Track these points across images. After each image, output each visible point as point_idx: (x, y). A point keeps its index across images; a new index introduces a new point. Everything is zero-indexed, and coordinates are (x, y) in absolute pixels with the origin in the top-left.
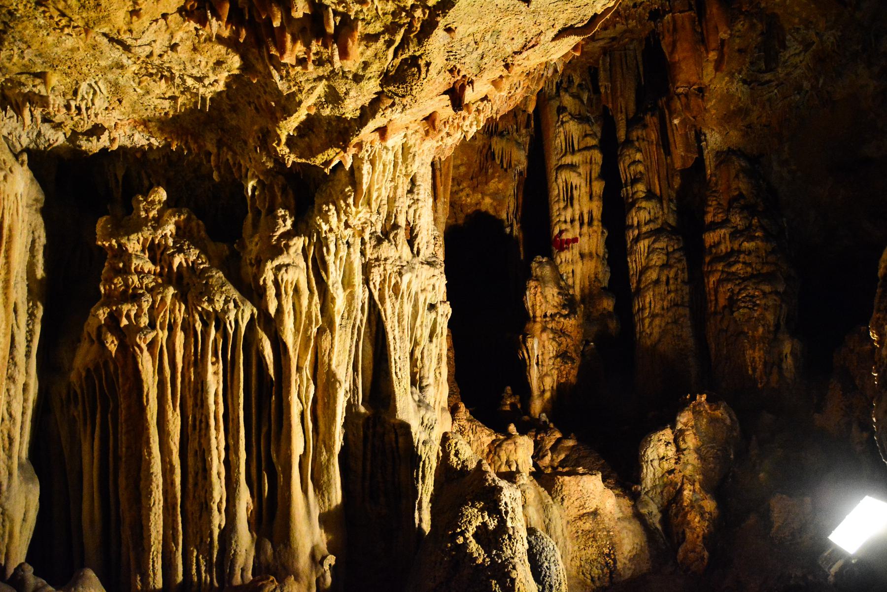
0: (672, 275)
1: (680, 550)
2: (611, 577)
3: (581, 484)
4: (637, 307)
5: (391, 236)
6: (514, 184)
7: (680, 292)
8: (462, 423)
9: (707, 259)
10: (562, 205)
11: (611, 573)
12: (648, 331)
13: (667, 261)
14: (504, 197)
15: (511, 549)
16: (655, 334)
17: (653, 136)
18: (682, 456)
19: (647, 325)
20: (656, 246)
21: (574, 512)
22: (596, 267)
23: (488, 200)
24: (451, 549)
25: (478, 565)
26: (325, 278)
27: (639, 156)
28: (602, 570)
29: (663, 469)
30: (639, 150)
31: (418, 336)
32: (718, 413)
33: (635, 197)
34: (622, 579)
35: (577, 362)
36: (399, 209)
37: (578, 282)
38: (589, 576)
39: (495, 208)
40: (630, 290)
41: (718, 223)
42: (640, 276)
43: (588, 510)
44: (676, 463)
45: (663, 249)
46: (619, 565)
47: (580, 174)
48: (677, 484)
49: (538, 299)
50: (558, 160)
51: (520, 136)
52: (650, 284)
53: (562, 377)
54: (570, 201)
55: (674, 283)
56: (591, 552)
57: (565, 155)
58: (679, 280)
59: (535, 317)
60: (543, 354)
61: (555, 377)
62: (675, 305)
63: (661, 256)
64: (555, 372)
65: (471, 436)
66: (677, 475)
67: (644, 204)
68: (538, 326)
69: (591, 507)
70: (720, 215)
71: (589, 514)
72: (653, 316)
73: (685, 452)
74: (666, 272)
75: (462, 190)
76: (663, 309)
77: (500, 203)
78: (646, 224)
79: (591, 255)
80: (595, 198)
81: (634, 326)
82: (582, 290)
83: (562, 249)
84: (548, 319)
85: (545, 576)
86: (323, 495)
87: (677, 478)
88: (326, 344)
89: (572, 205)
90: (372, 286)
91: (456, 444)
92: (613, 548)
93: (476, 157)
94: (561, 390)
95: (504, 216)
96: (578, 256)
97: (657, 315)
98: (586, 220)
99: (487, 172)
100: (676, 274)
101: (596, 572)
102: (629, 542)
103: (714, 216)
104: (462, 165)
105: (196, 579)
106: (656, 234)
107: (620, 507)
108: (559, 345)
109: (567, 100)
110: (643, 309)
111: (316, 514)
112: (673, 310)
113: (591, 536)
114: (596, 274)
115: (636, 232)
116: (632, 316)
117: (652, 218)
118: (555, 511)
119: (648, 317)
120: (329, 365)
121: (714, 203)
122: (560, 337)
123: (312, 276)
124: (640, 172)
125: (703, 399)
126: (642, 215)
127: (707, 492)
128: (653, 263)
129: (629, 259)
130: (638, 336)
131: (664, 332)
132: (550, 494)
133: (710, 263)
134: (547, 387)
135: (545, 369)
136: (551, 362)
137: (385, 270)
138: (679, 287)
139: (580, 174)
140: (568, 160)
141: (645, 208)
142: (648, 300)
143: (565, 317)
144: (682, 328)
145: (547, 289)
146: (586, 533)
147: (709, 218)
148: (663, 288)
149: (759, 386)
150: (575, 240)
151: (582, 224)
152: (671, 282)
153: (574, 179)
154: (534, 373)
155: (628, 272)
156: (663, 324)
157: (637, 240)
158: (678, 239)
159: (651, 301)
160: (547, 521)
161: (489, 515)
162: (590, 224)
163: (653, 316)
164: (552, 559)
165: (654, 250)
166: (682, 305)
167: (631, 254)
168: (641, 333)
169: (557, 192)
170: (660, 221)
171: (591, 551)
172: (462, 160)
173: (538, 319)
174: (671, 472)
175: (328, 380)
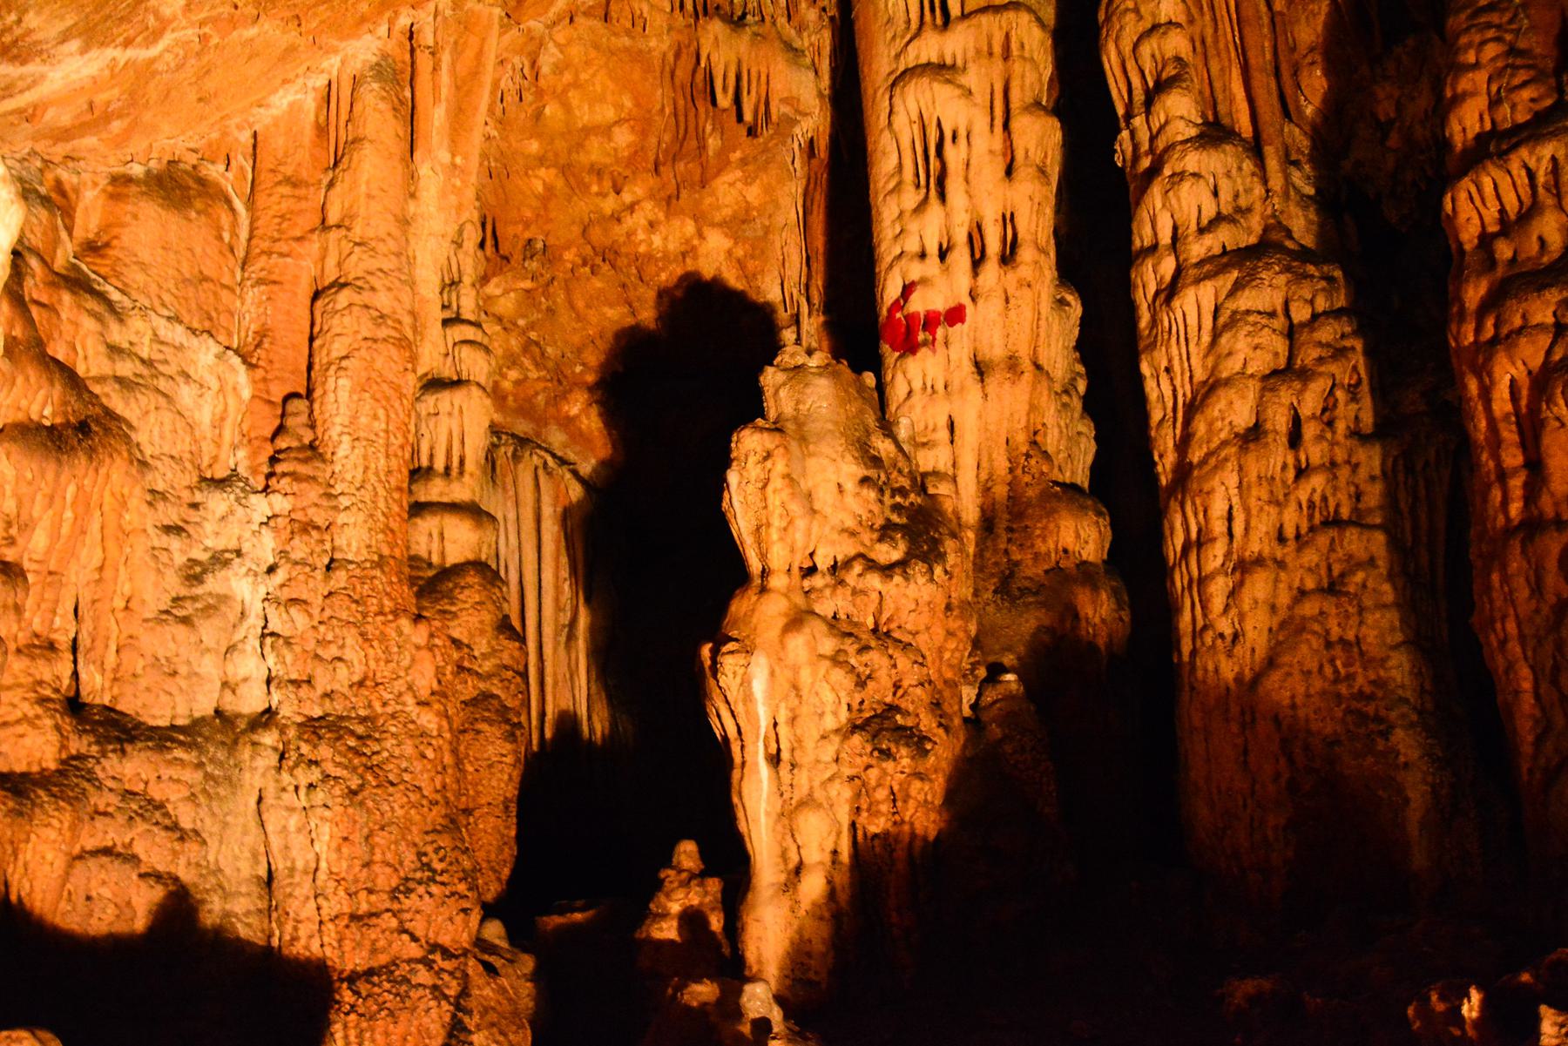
0: (1310, 403)
4: (1179, 540)
6: (796, 188)
7: (1344, 473)
9: (1474, 293)
10: (911, 198)
13: (1291, 357)
14: (767, 230)
16: (1251, 634)
19: (1218, 603)
20: (1245, 301)
22: (1033, 408)
33: (1161, 144)
34: (824, 986)
35: (944, 751)
37: (968, 461)
39: (741, 264)
40: (1156, 478)
41: (1517, 128)
42: (1187, 422)
49: (774, 501)
50: (898, 56)
51: (800, 29)
52: (1224, 443)
53: (873, 812)
55: (1320, 438)
58: (1341, 426)
59: (765, 573)
60: (793, 720)
62: (1326, 523)
63: (1265, 337)
64: (842, 794)
67: (1192, 161)
70: (1526, 94)
72: (1243, 567)
74: (1286, 396)
75: (631, 208)
76: (1281, 539)
77: (759, 247)
78: (1201, 231)
80: (1023, 172)
81: (1170, 610)
83: (909, 347)
84: (818, 581)
89: (942, 196)
93: (660, 96)
94: (873, 869)
95: (773, 294)
96: (968, 367)
97: (1259, 561)
98: (993, 246)
99: (702, 147)
100: (1329, 406)
103: (1494, 103)
108: (861, 683)
110: (1201, 542)
112: (1323, 540)
115: (1168, 266)
116: (1163, 572)
117: (1226, 209)
119: (1222, 569)
121: (1491, 50)
122: (865, 649)
124: (1178, 59)
126: (1189, 199)
128: (1234, 365)
129: (1145, 369)
130: (1186, 646)
131: (1289, 629)
133: (1493, 302)
135: (802, 778)
136: (828, 752)
138: (1340, 455)
140: (930, 48)
142: (1218, 508)
143: (887, 570)
144: (1361, 610)
145: (812, 463)
147: (1468, 122)
148: (1277, 456)
150: (955, 315)
152: (1310, 431)
153: (944, 105)
155: (1145, 416)
156: (1284, 599)
157: (1170, 291)
158: (1330, 279)
165: (1235, 319)
166: (1358, 521)
167: (1152, 346)
168: (1197, 634)
170: (1256, 222)
172: (619, 107)
173: (777, 582)
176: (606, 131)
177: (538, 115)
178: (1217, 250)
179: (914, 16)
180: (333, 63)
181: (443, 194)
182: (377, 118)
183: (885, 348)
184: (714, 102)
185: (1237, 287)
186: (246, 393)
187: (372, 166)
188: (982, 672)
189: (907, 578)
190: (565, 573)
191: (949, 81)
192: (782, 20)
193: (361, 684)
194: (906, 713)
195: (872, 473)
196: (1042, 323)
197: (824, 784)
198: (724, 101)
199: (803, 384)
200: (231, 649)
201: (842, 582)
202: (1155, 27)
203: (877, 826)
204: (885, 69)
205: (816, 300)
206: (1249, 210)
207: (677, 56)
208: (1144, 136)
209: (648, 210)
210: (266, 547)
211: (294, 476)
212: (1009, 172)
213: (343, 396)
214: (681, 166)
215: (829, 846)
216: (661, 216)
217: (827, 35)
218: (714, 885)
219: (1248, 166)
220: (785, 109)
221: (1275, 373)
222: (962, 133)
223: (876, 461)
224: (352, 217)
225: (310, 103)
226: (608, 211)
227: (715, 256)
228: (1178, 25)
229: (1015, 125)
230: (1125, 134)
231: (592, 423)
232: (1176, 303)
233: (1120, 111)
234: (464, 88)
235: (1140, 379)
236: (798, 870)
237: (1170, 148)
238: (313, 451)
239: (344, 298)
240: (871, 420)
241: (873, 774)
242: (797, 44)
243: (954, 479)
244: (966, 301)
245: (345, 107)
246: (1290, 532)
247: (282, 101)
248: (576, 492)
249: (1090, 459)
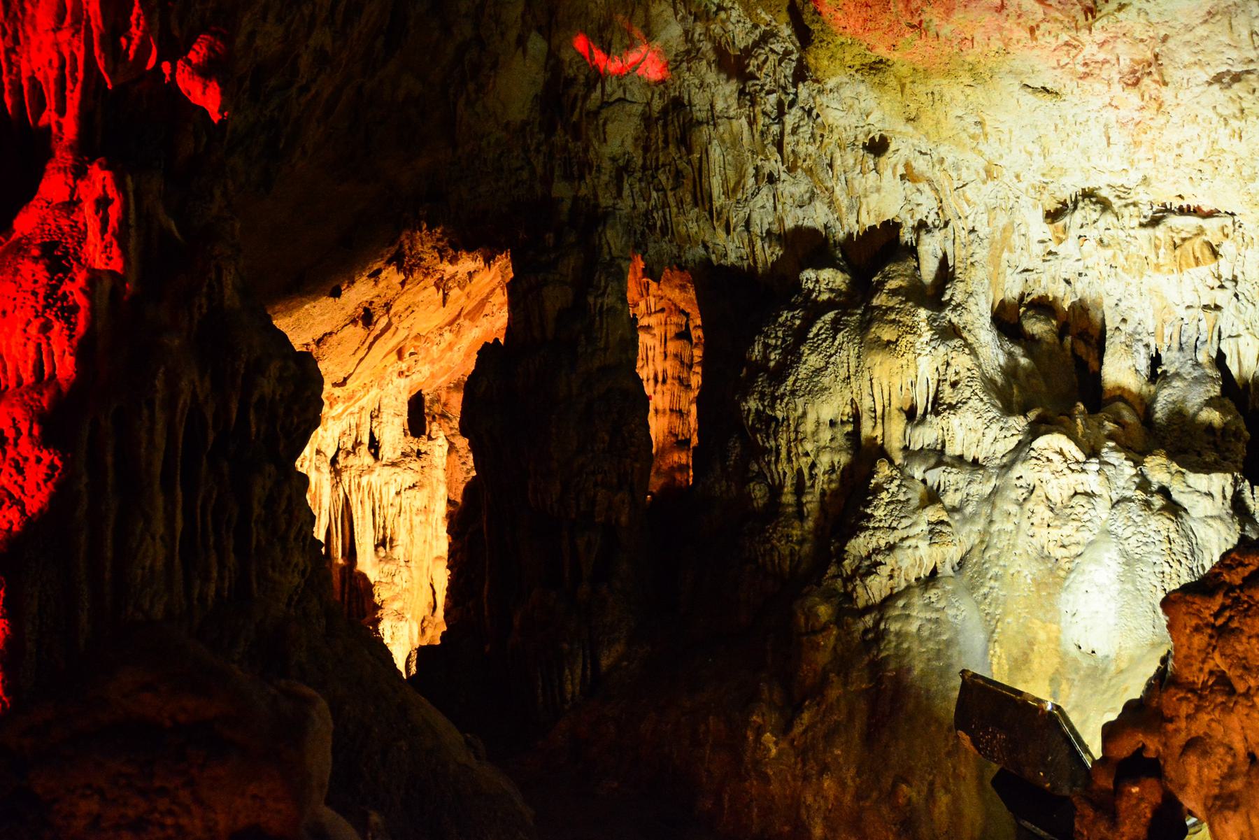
79: (664, 412)
98: (660, 379)
162: (664, 381)
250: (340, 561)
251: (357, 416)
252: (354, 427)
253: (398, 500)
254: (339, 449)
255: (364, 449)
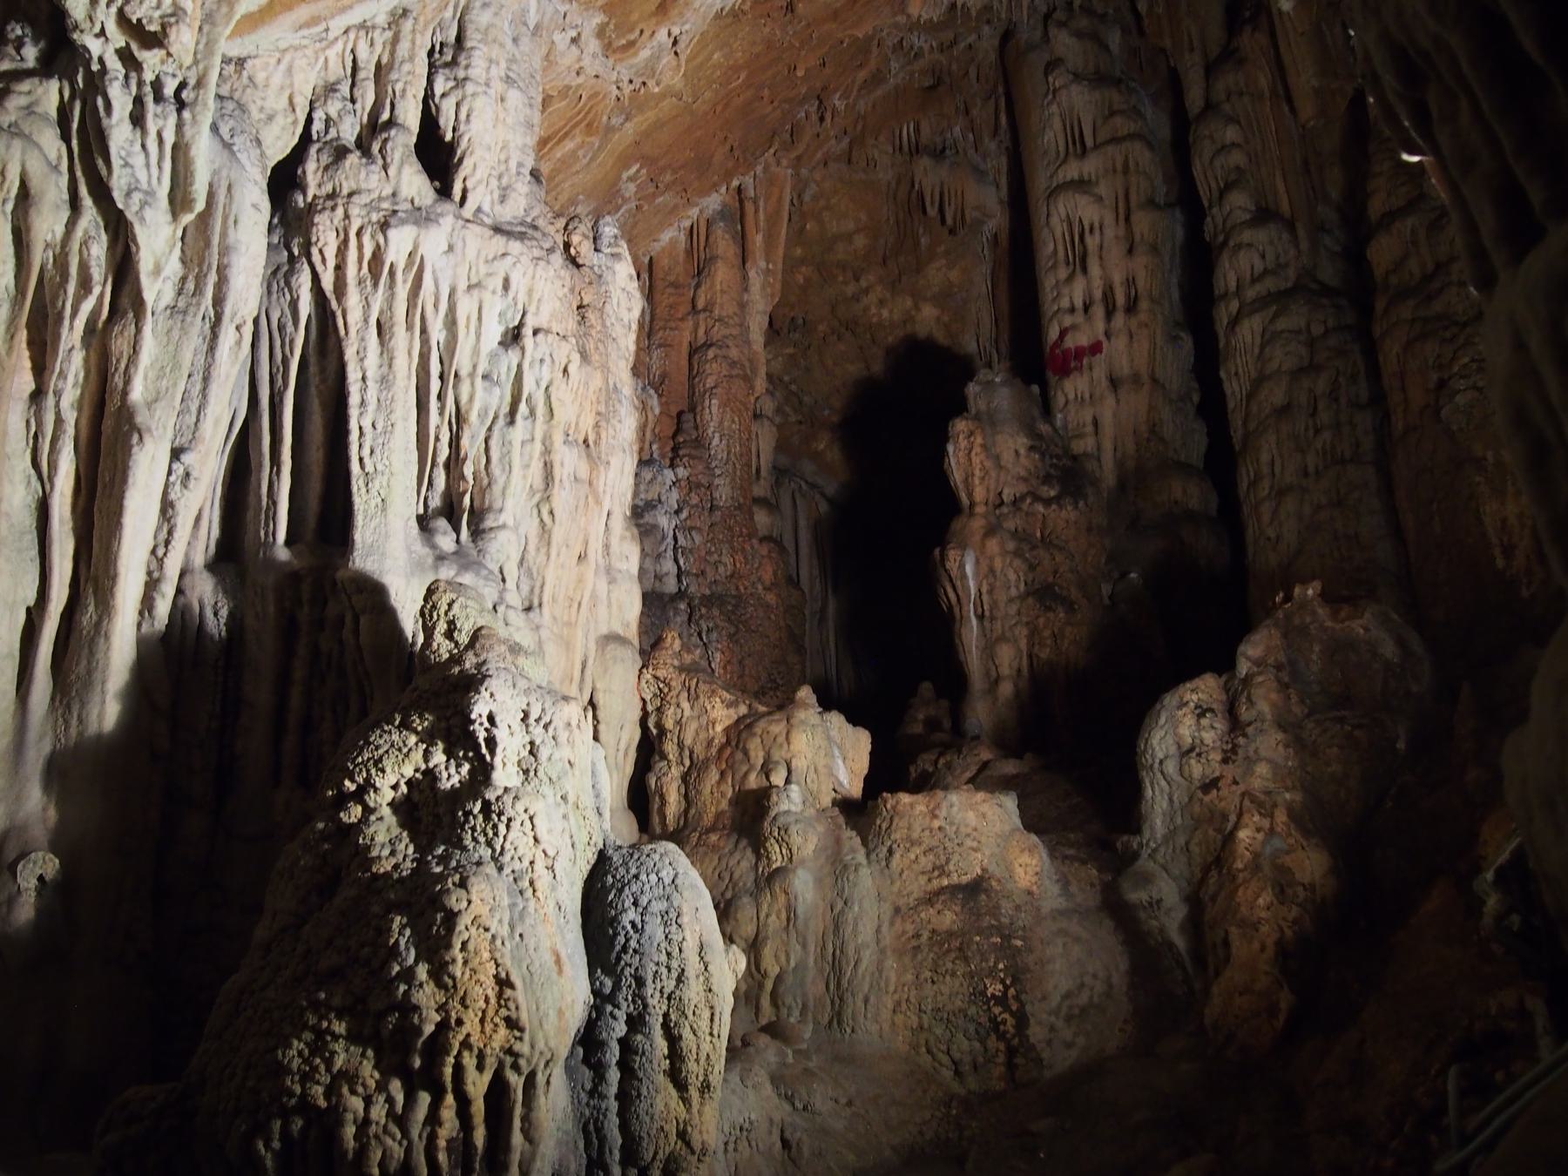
0: (1322, 384)
1: (1215, 990)
2: (1010, 1066)
3: (943, 813)
5: (376, 147)
6: (985, 269)
8: (661, 673)
10: (1063, 273)
11: (1011, 1052)
12: (1271, 533)
15: (489, 844)
17: (1264, 81)
18: (1241, 740)
19: (1266, 518)
20: (1282, 324)
21: (917, 886)
22: (1151, 408)
23: (928, 312)
24: (324, 836)
25: (376, 877)
26: (104, 172)
27: (1231, 134)
28: (983, 1042)
29: (1190, 779)
30: (1232, 120)
31: (464, 399)
32: (1357, 627)
33: (1229, 225)
34: (1048, 1074)
36: (399, 87)
37: (1108, 445)
38: (945, 1059)
43: (955, 879)
44: (1225, 761)
45: (1299, 332)
46: (1036, 1033)
47: (1100, 199)
48: (1225, 817)
49: (976, 460)
51: (984, 157)
54: (1081, 263)
56: (951, 990)
57: (1064, 161)
59: (972, 505)
60: (990, 592)
61: (1023, 644)
64: (1022, 633)
65: (686, 705)
66: (1224, 792)
67: (1247, 236)
68: (977, 524)
69: (966, 868)
71: (954, 889)
73: (1250, 730)
75: (866, 291)
78: (1254, 281)
79: (1136, 379)
82: (1120, 464)
83: (1065, 371)
84: (1005, 510)
85: (624, 949)
86: (68, 707)
87: (1228, 798)
88: (120, 344)
89: (1084, 270)
90: (316, 258)
91: (450, 605)
92: (1015, 980)
95: (972, 347)
96: (1105, 383)
98: (1120, 299)
99: (917, 244)
101: (965, 1044)
102: (1073, 967)
104: (858, 231)
105: (350, 1144)
106: (1279, 300)
107: (1064, 882)
108: (1032, 568)
109: (1064, 42)
111: (38, 751)
113: (951, 945)
114: (1154, 428)
115: (1234, 305)
118: (866, 879)
120: (125, 393)
122: (1034, 548)
123: (79, 174)
124: (1238, 168)
125: (1310, 592)
127: (1306, 833)
129: (1223, 374)
132: (865, 843)
134: (1005, 671)
135: (998, 625)
137: (347, 216)
139: (1100, 199)
140: (1072, 171)
141: (1250, 245)
142: (1265, 457)
143: (1047, 502)
145: (999, 438)
146: (939, 938)
149: (1525, 593)
151: (1109, 314)
153: (1086, 210)
154: (971, 634)
157: (1234, 322)
159: (1269, 460)
160: (840, 905)
161: (449, 754)
162: (1131, 308)
163: (1280, 493)
164: (658, 907)
169: (1051, 247)
170: (1291, 273)
171: (948, 985)
173: (980, 509)
174: (1210, 785)
175: (118, 427)
176: (849, 237)
177: (803, 228)
178: (1264, 293)
179: (1062, 149)
180: (694, 212)
181: (763, 288)
182: (724, 244)
183: (1049, 374)
184: (925, 212)
185: (1276, 316)
186: (657, 411)
187: (722, 274)
188: (1116, 575)
189: (1061, 507)
190: (816, 572)
191: (1085, 193)
192: (971, 152)
193: (732, 576)
194: (1061, 588)
195: (1037, 443)
196: (1158, 351)
197: (1011, 628)
198: (932, 212)
199: (994, 391)
200: (659, 556)
201: (1019, 509)
202: (1223, 147)
203: (1045, 654)
204: (1043, 186)
205: (1004, 349)
206: (1287, 265)
207: (898, 183)
208: (1219, 221)
209: (879, 291)
210: (673, 497)
211: (691, 457)
212: (1130, 251)
213: (714, 409)
214: (902, 259)
215: (1015, 665)
216: (888, 295)
217: (1004, 160)
218: (945, 703)
219: (1285, 236)
220: (976, 214)
221: (1301, 370)
222: (1097, 225)
223: (1040, 437)
224: (713, 305)
225: (683, 237)
226: (850, 294)
227: (928, 321)
228: (1238, 146)
229: (1135, 218)
230: (1209, 219)
231: (834, 455)
232: (1237, 329)
233: (1206, 204)
234: (773, 221)
235: (1220, 381)
236: (997, 681)
237: (1233, 227)
238: (700, 443)
239: (711, 353)
240: (1036, 412)
241: (1041, 620)
242: (982, 167)
243: (1099, 460)
244: (1102, 338)
245: (703, 239)
246: (1311, 469)
247: (666, 236)
248: (824, 507)
249: (1203, 449)
250: (282, 554)
251: (381, 38)
252: (367, 72)
253: (513, 356)
254: (306, 139)
255: (403, 142)
